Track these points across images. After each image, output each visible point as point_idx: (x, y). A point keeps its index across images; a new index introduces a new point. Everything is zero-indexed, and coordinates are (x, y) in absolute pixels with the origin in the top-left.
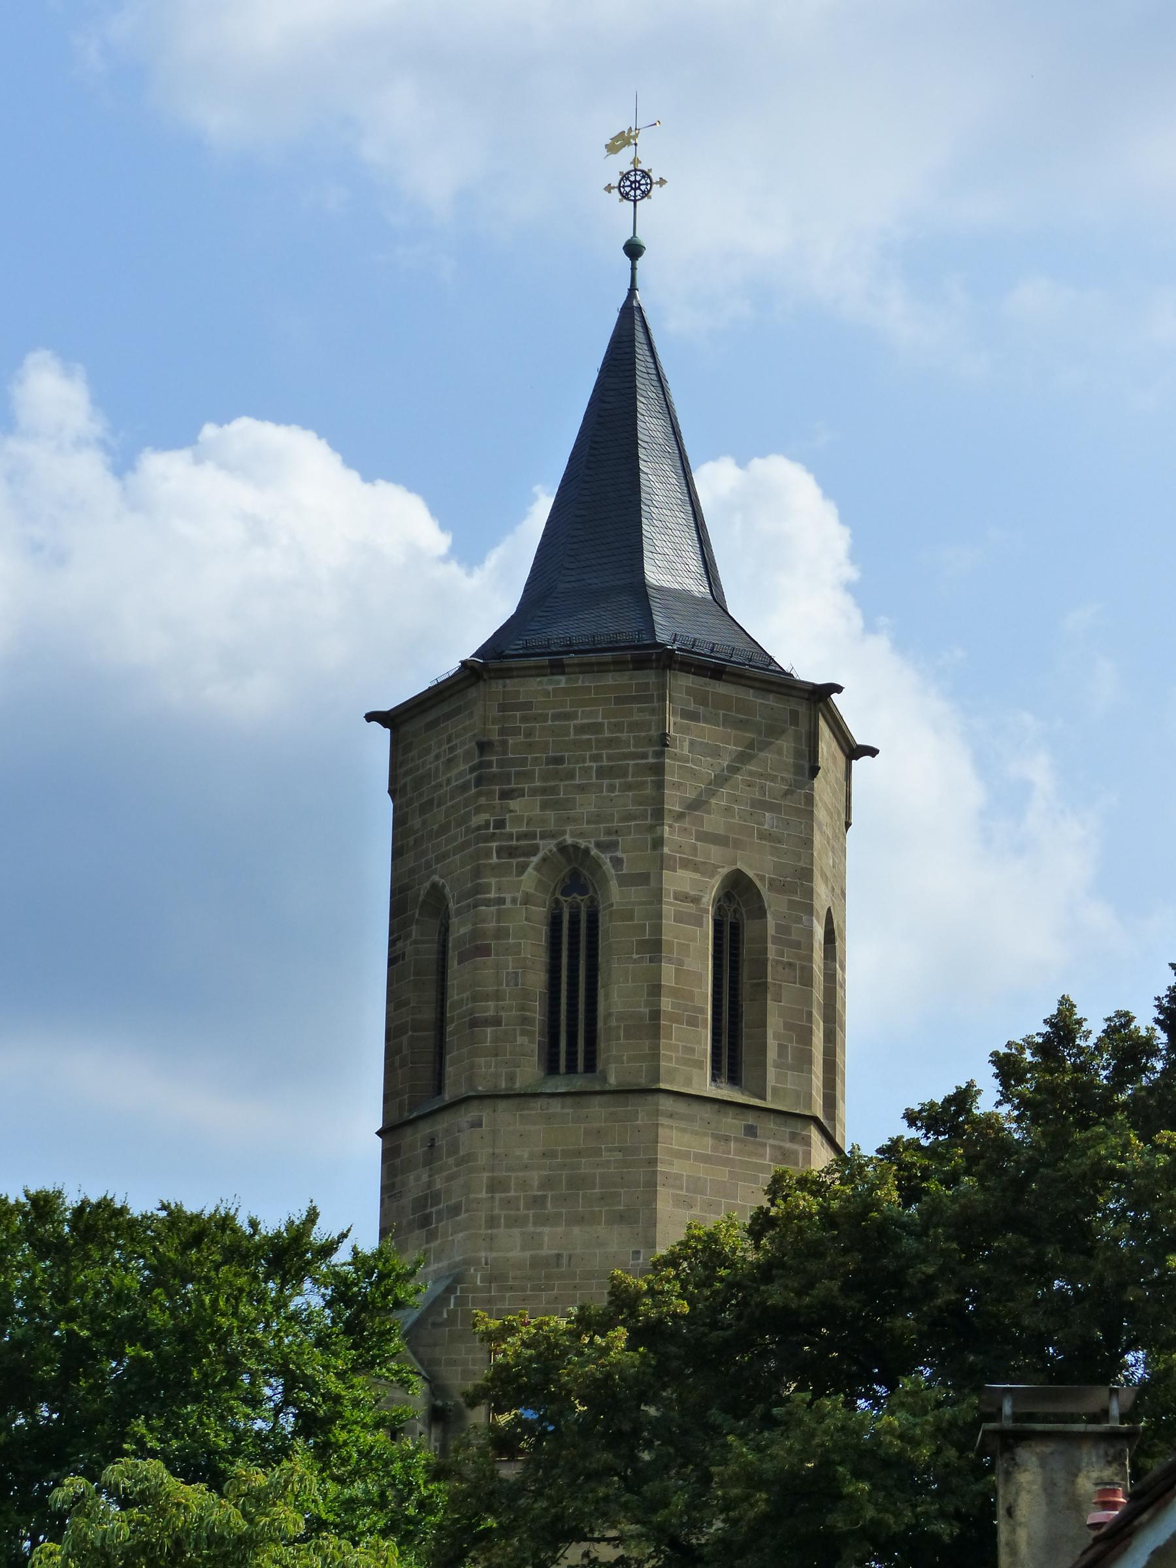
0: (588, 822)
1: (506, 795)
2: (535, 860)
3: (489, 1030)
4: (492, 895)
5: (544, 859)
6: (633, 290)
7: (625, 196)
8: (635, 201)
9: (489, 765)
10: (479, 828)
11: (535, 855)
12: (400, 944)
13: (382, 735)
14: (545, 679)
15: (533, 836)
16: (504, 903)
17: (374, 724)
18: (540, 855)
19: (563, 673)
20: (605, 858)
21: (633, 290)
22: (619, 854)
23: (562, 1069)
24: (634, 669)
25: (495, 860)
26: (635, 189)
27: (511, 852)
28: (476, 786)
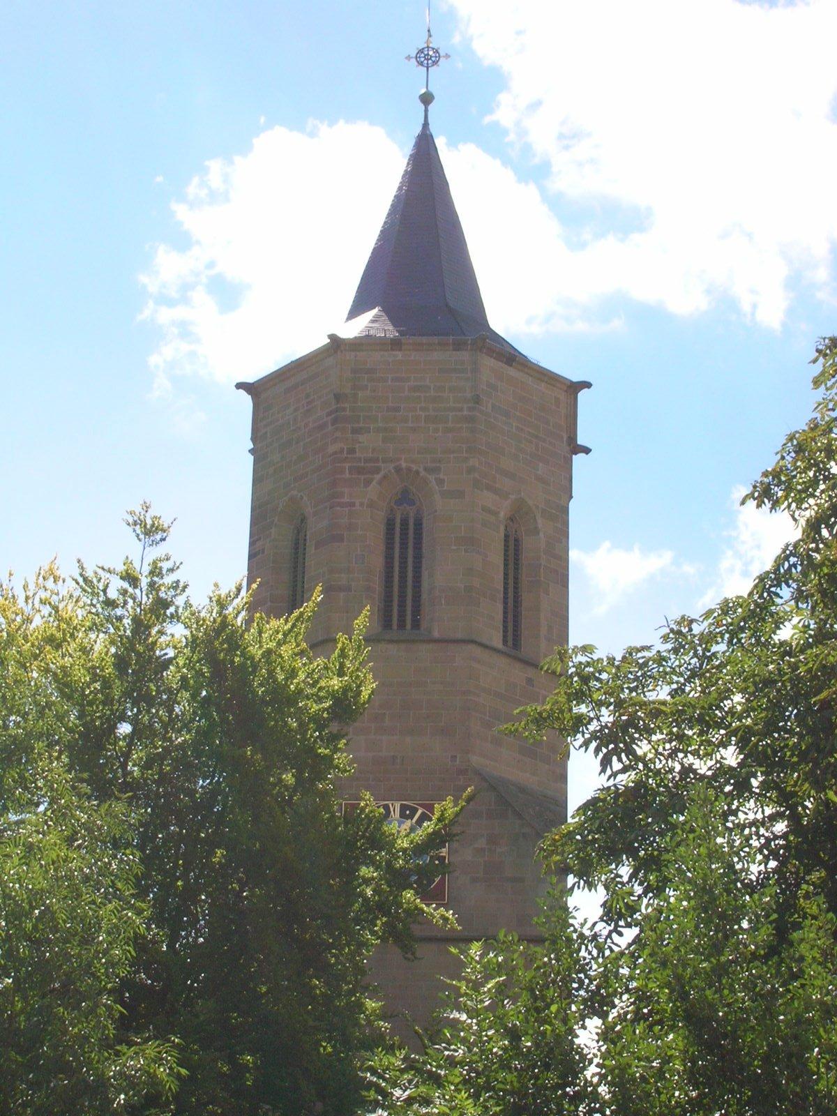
0: (419, 453)
1: (355, 431)
2: (378, 477)
3: (342, 594)
4: (346, 499)
5: (385, 477)
6: (426, 125)
7: (421, 64)
8: (428, 68)
9: (344, 409)
10: (335, 453)
11: (378, 473)
12: (259, 544)
13: (246, 400)
14: (386, 353)
15: (377, 460)
16: (354, 506)
17: (242, 392)
18: (382, 473)
19: (400, 350)
20: (432, 478)
21: (426, 125)
22: (441, 476)
23: (395, 627)
24: (454, 350)
25: (347, 475)
26: (428, 60)
27: (360, 471)
28: (332, 425)
